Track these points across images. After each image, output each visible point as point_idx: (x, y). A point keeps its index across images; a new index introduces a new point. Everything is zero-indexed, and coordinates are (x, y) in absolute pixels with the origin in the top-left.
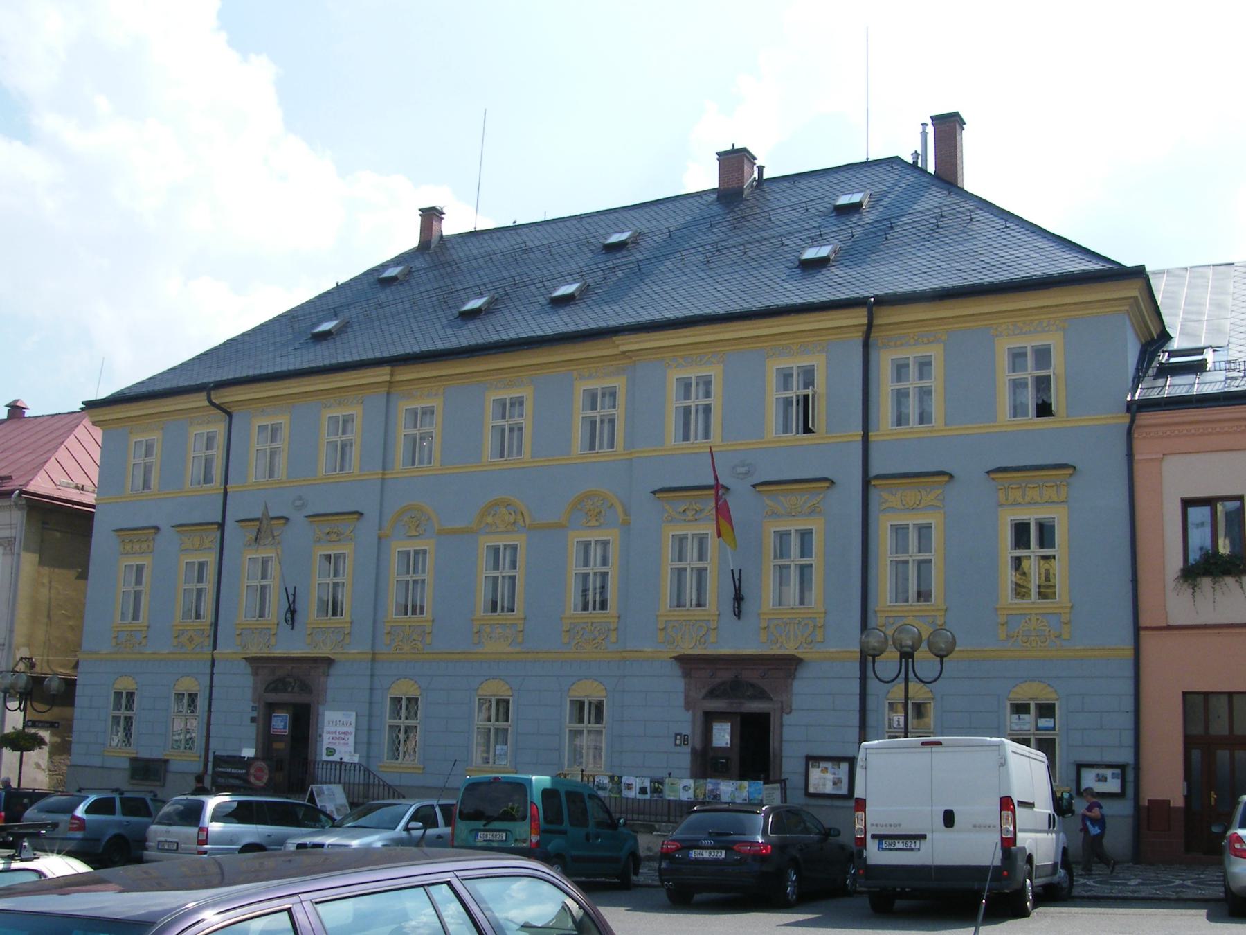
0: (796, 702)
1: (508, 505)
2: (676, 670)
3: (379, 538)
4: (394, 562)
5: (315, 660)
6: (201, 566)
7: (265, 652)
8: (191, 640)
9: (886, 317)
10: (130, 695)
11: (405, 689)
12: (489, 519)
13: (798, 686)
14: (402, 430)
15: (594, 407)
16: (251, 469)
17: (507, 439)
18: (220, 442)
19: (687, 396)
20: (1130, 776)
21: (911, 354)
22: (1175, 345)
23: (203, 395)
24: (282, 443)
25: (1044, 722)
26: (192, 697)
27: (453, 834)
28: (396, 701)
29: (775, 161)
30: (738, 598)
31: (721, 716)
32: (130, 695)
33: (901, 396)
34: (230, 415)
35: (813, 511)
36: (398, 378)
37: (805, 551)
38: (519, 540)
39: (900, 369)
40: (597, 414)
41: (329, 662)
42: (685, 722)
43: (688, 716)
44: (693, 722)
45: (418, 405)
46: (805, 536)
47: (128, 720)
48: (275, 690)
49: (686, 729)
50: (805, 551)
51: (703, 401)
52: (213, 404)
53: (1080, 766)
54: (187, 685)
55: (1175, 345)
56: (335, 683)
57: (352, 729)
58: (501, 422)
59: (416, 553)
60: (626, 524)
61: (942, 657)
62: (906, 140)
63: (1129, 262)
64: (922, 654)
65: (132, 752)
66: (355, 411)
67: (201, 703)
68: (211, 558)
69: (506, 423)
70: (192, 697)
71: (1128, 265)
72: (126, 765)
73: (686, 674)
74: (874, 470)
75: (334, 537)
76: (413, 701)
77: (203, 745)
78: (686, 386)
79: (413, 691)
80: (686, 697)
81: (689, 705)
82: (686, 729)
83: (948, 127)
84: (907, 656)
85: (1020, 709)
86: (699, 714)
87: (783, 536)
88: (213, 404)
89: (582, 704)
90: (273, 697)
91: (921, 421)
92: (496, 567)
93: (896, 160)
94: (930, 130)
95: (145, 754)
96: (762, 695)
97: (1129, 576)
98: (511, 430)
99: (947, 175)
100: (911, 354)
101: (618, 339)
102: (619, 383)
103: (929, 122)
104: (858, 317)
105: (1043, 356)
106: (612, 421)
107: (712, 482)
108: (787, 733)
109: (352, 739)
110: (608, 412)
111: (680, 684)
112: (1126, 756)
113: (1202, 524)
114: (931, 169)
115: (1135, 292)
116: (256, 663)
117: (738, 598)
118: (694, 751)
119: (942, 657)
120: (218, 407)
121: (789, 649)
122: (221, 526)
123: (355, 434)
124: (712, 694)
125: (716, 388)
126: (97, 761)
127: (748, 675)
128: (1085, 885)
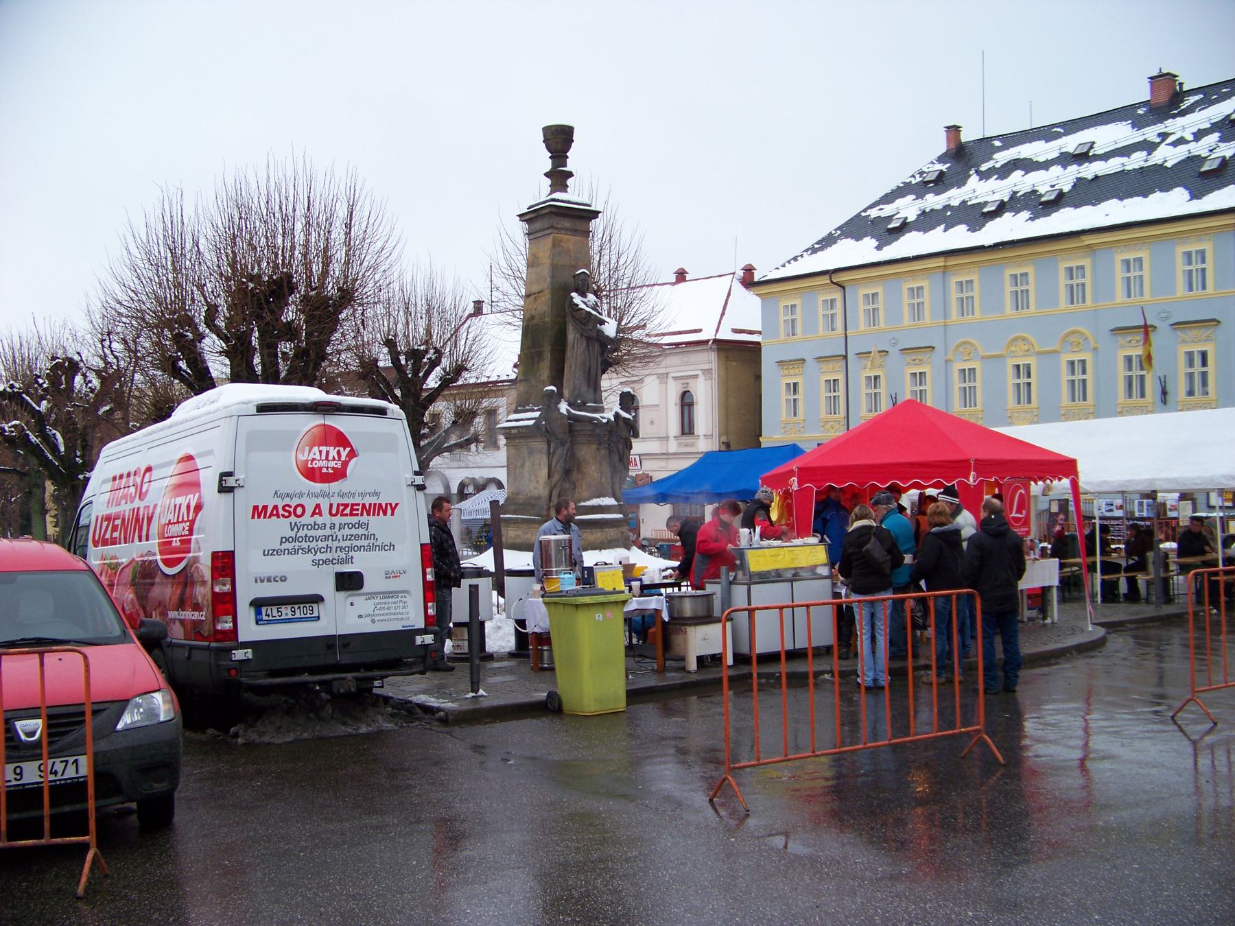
1: (1024, 339)
3: (947, 361)
4: (956, 376)
8: (832, 427)
12: (1013, 348)
14: (954, 294)
15: (1072, 278)
16: (860, 324)
17: (917, 310)
18: (839, 304)
19: (1190, 263)
23: (827, 277)
24: (880, 305)
30: (1164, 393)
34: (844, 288)
37: (1204, 363)
38: (1031, 360)
40: (1074, 282)
45: (963, 279)
46: (1204, 355)
50: (1204, 363)
51: (1201, 266)
58: (1015, 289)
66: (924, 283)
68: (841, 377)
69: (1019, 289)
78: (1188, 255)
87: (1190, 355)
92: (1073, 373)
101: (1083, 238)
102: (1086, 262)
107: (1142, 323)
110: (1080, 281)
113: (968, 396)
117: (1164, 393)
122: (845, 357)
123: (926, 299)
125: (1209, 257)
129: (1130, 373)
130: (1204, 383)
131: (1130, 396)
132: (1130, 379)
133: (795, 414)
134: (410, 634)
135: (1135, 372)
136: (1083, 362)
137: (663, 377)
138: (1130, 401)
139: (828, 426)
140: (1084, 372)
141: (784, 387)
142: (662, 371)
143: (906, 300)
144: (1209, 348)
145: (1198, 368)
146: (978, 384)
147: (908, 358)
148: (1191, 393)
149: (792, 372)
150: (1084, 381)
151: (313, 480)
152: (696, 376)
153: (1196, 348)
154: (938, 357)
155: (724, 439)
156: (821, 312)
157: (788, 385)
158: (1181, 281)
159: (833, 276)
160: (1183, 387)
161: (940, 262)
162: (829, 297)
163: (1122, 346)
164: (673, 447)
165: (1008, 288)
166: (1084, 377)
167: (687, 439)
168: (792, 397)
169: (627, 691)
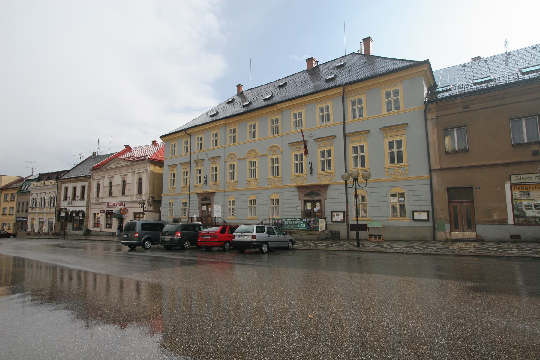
0: (328, 196)
1: (254, 150)
2: (295, 190)
5: (211, 193)
6: (187, 172)
9: (348, 89)
10: (233, 201)
11: (232, 199)
13: (328, 192)
16: (195, 148)
20: (431, 214)
21: (356, 98)
22: (439, 87)
25: (401, 199)
26: (186, 203)
27: (188, 240)
28: (230, 201)
29: (321, 59)
30: (312, 170)
32: (173, 204)
33: (354, 111)
35: (331, 144)
39: (354, 103)
41: (214, 193)
42: (299, 203)
43: (300, 202)
44: (301, 203)
47: (172, 210)
49: (299, 205)
53: (413, 212)
54: (184, 201)
55: (439, 87)
56: (216, 198)
60: (282, 153)
61: (367, 180)
63: (421, 59)
64: (360, 179)
65: (173, 217)
67: (187, 205)
68: (188, 170)
70: (186, 203)
71: (421, 60)
72: (172, 220)
73: (299, 191)
74: (347, 132)
80: (299, 197)
81: (300, 199)
82: (299, 205)
83: (367, 41)
84: (356, 179)
85: (393, 195)
86: (303, 202)
87: (323, 153)
90: (203, 202)
91: (360, 116)
93: (353, 53)
94: (363, 43)
95: (176, 218)
96: (318, 195)
97: (427, 154)
99: (367, 54)
101: (278, 105)
103: (362, 41)
104: (340, 90)
111: (297, 193)
112: (429, 208)
114: (363, 53)
115: (426, 69)
116: (198, 194)
117: (312, 170)
119: (367, 180)
121: (325, 182)
122: (190, 162)
124: (305, 196)
128: (418, 249)
130: (329, 165)
131: (297, 172)
133: (216, 181)
135: (299, 161)
137: (133, 173)
141: (211, 169)
142: (133, 171)
143: (229, 134)
144: (403, 138)
145: (326, 158)
147: (211, 162)
148: (323, 169)
150: (278, 167)
152: (143, 172)
153: (325, 149)
154: (222, 161)
155: (152, 195)
156: (212, 139)
157: (213, 168)
158: (319, 119)
160: (320, 167)
161: (223, 122)
162: (186, 140)
163: (293, 151)
164: (135, 199)
165: (270, 125)
167: (139, 196)
168: (232, 171)
169: (23, 259)
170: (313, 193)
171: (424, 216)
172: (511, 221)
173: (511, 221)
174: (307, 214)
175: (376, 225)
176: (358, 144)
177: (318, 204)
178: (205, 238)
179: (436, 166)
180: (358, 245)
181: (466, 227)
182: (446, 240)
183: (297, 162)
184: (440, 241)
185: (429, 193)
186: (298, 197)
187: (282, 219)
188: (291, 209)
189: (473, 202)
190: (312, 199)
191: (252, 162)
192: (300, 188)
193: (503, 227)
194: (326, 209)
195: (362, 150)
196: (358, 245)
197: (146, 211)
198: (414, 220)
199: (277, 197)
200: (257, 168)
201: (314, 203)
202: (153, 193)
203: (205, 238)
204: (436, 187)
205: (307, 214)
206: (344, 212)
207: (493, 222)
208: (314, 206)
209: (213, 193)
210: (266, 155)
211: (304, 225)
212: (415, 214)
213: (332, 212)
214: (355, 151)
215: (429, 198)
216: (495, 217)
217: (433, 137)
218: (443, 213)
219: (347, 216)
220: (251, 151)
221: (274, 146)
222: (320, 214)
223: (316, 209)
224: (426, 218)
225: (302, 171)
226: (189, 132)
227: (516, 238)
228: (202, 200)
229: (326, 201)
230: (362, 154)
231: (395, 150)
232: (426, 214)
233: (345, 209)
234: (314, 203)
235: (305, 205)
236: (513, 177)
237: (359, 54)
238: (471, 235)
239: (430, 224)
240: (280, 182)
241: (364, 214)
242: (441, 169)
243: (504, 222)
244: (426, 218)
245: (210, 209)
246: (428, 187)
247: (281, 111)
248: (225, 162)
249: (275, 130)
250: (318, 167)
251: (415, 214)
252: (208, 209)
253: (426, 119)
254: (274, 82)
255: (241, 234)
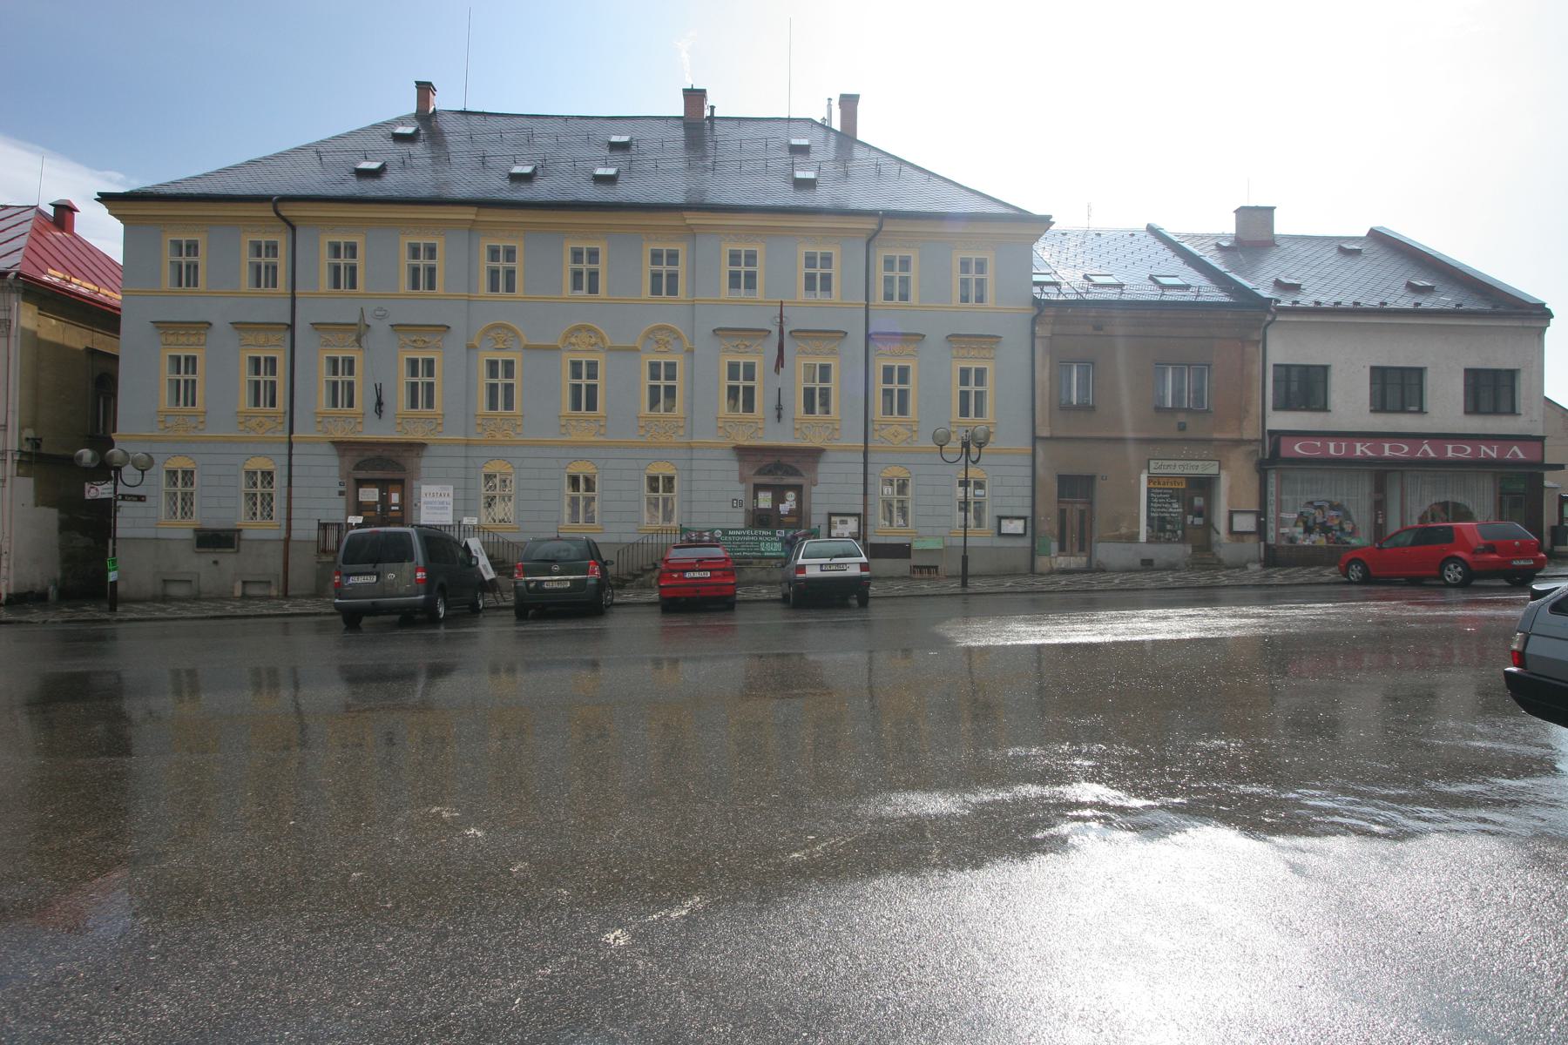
0: (820, 478)
2: (332, 451)
7: (352, 437)
9: (889, 226)
13: (424, 462)
23: (269, 206)
25: (978, 492)
29: (722, 104)
30: (379, 403)
31: (765, 487)
34: (294, 228)
35: (832, 352)
36: (480, 218)
37: (430, 373)
39: (889, 263)
42: (740, 491)
43: (742, 487)
48: (770, 472)
52: (278, 215)
53: (1000, 518)
57: (450, 500)
59: (187, 358)
60: (691, 352)
62: (815, 104)
67: (279, 481)
72: (190, 535)
75: (420, 344)
76: (669, 480)
77: (284, 516)
79: (188, 465)
81: (742, 480)
82: (741, 496)
88: (278, 215)
89: (175, 472)
90: (362, 475)
95: (213, 525)
96: (796, 473)
97: (1029, 405)
98: (188, 267)
99: (847, 138)
100: (898, 254)
101: (687, 214)
102: (681, 248)
105: (981, 266)
106: (275, 268)
108: (815, 499)
109: (450, 508)
112: (1027, 512)
117: (779, 408)
118: (747, 511)
120: (284, 219)
121: (816, 443)
122: (291, 327)
124: (760, 472)
126: (150, 533)
127: (786, 460)
129: (414, 380)
132: (414, 386)
134: (1108, 815)
136: (273, 360)
138: (734, 415)
139: (253, 422)
140: (273, 373)
144: (988, 366)
146: (199, 378)
149: (183, 339)
150: (351, 384)
151: (1456, 505)
155: (29, 433)
159: (280, 206)
161: (469, 214)
166: (350, 378)
170: (778, 468)
171: (1016, 527)
172: (1143, 537)
173: (1143, 537)
174: (761, 520)
175: (931, 544)
176: (897, 363)
177: (791, 496)
178: (688, 575)
179: (1043, 432)
180: (964, 584)
181: (1076, 549)
182: (1052, 572)
183: (334, 378)
184: (1042, 574)
185: (1028, 482)
186: (736, 475)
187: (712, 531)
188: (716, 501)
189: (1091, 503)
190: (777, 482)
191: (179, 358)
192: (744, 453)
193: (1134, 546)
194: (815, 509)
195: (509, 373)
196: (964, 584)
197: (124, 497)
198: (1000, 534)
199: (669, 472)
200: (435, 380)
201: (779, 493)
202: (34, 425)
203: (688, 575)
204: (1040, 471)
205: (761, 520)
206: (858, 515)
207: (1119, 539)
208: (779, 498)
209: (417, 447)
210: (635, 350)
211: (778, 546)
212: (1004, 522)
213: (831, 515)
214: (888, 377)
215: (1028, 491)
216: (1124, 530)
217: (1043, 374)
218: (1048, 524)
219: (865, 525)
220: (578, 329)
221: (660, 328)
222: (794, 520)
223: (784, 508)
224: (1021, 531)
225: (351, 404)
226: (288, 211)
227: (1147, 564)
228: (358, 467)
229: (814, 489)
230: (509, 381)
231: (972, 388)
232: (1020, 523)
233: (860, 510)
234: (779, 493)
235: (756, 497)
236: (1152, 463)
237: (822, 126)
238: (1078, 561)
239: (1026, 542)
240: (681, 432)
241: (901, 522)
242: (1051, 438)
243: (1133, 538)
244: (1021, 531)
245: (395, 498)
246: (1028, 471)
247: (691, 233)
248: (470, 347)
249: (665, 284)
250: (398, 400)
251: (1004, 522)
252: (385, 500)
253: (1033, 334)
254: (566, 118)
255: (827, 561)
